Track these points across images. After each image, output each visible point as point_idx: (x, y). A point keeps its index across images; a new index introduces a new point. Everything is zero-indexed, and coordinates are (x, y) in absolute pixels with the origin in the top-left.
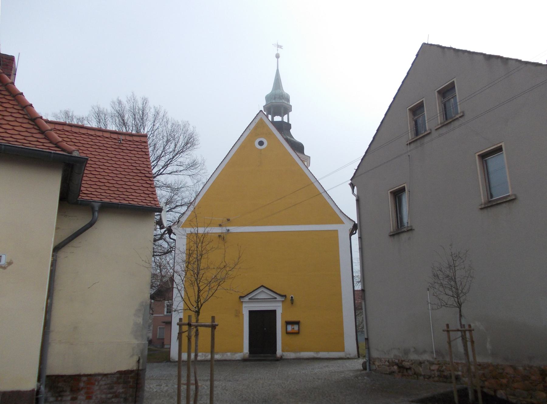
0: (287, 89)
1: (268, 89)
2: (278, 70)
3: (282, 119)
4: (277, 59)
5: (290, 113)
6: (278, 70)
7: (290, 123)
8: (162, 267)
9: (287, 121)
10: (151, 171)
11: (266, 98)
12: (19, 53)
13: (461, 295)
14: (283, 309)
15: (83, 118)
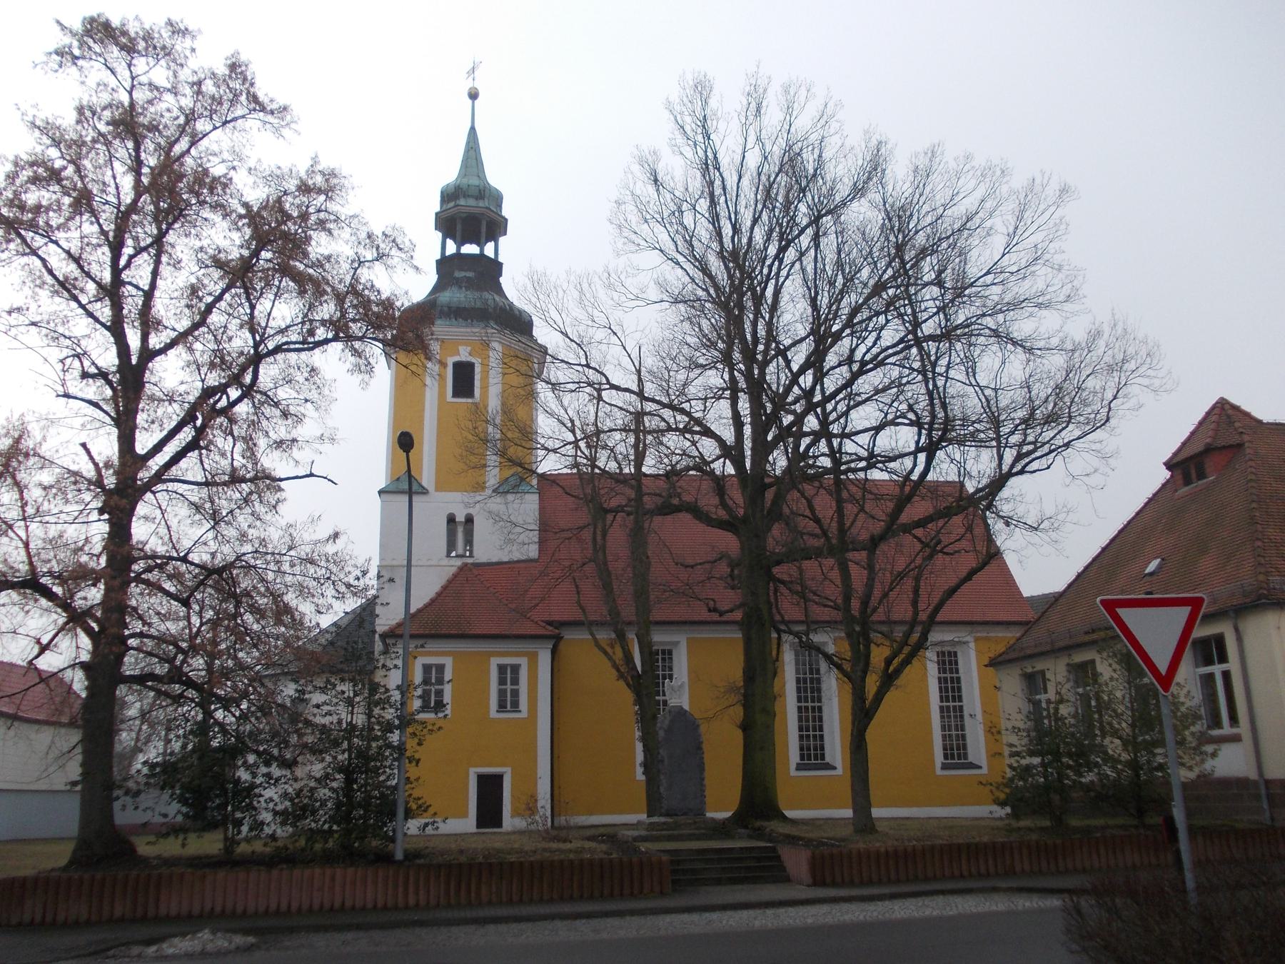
0: (495, 177)
1: (449, 173)
2: (473, 129)
3: (482, 250)
4: (470, 102)
5: (502, 240)
6: (473, 129)
7: (500, 260)
8: (206, 330)
9: (492, 256)
10: (202, 203)
11: (442, 193)
12: (58, 22)
13: (831, 418)
14: (454, 663)
15: (331, 198)
